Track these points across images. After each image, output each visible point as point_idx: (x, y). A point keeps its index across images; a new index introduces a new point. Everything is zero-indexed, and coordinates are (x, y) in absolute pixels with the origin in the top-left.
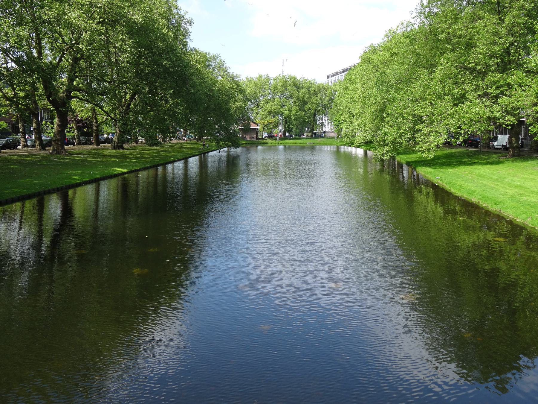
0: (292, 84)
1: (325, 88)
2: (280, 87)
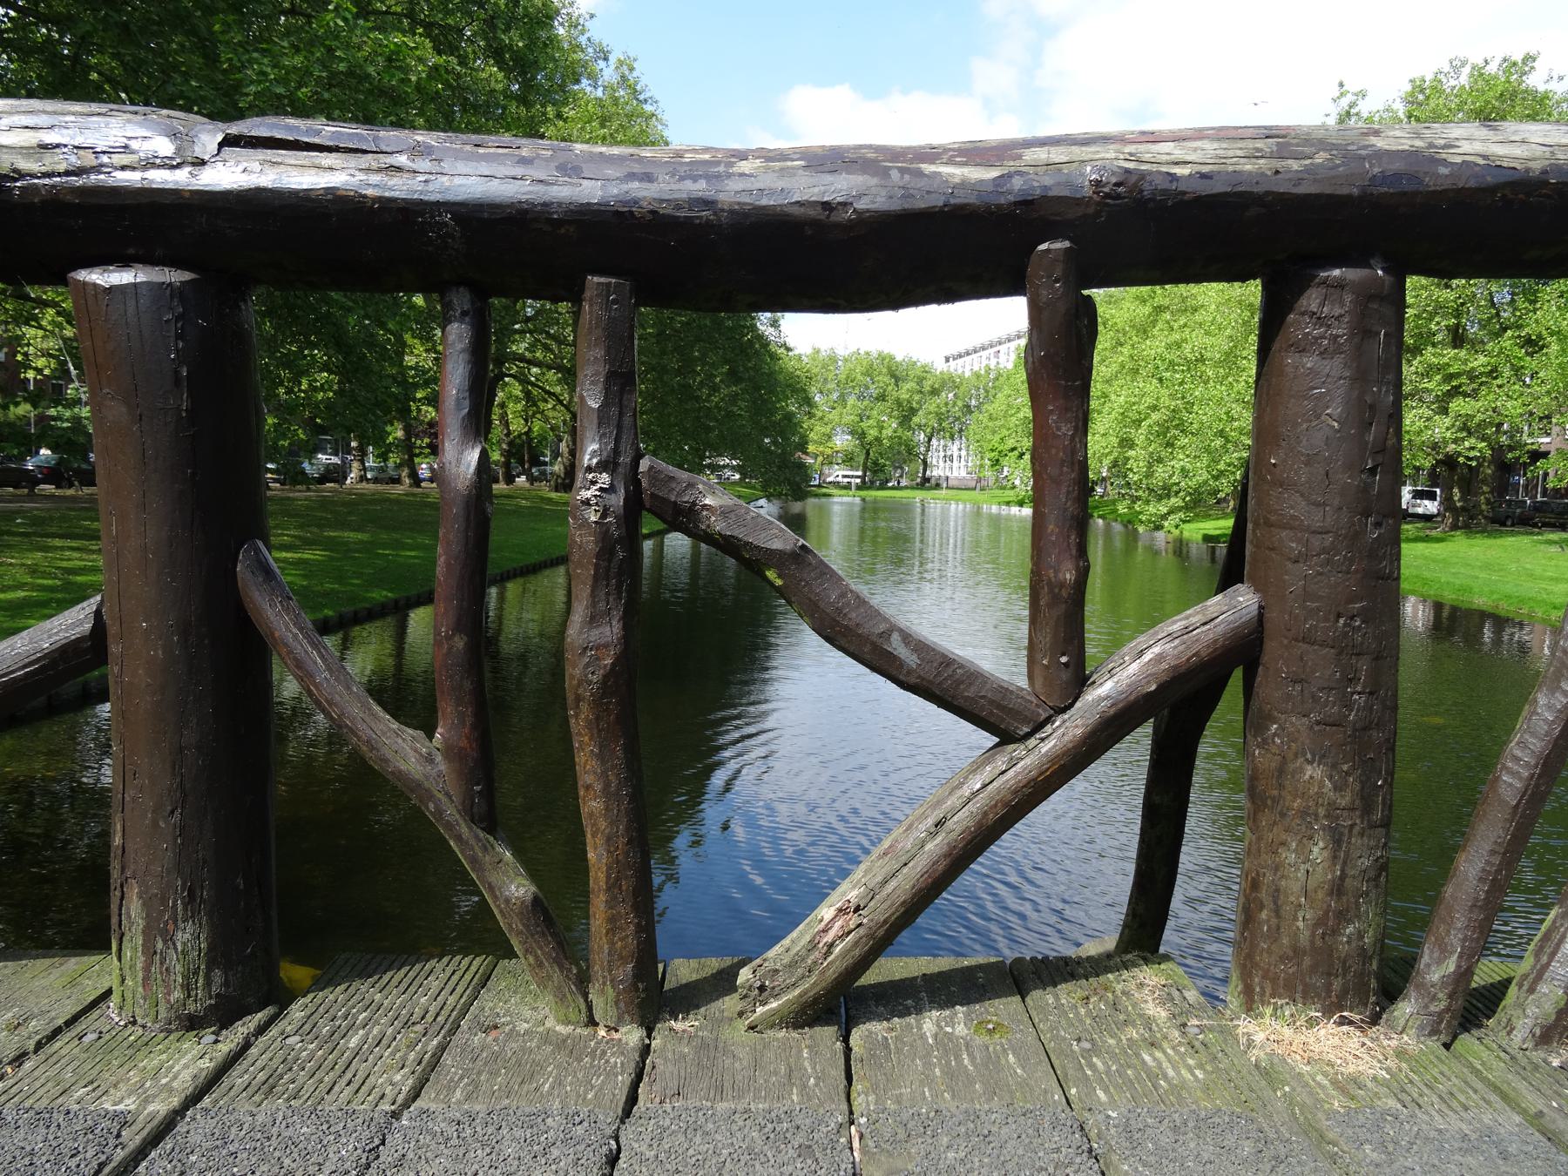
0: (885, 370)
1: (954, 382)
2: (859, 377)
